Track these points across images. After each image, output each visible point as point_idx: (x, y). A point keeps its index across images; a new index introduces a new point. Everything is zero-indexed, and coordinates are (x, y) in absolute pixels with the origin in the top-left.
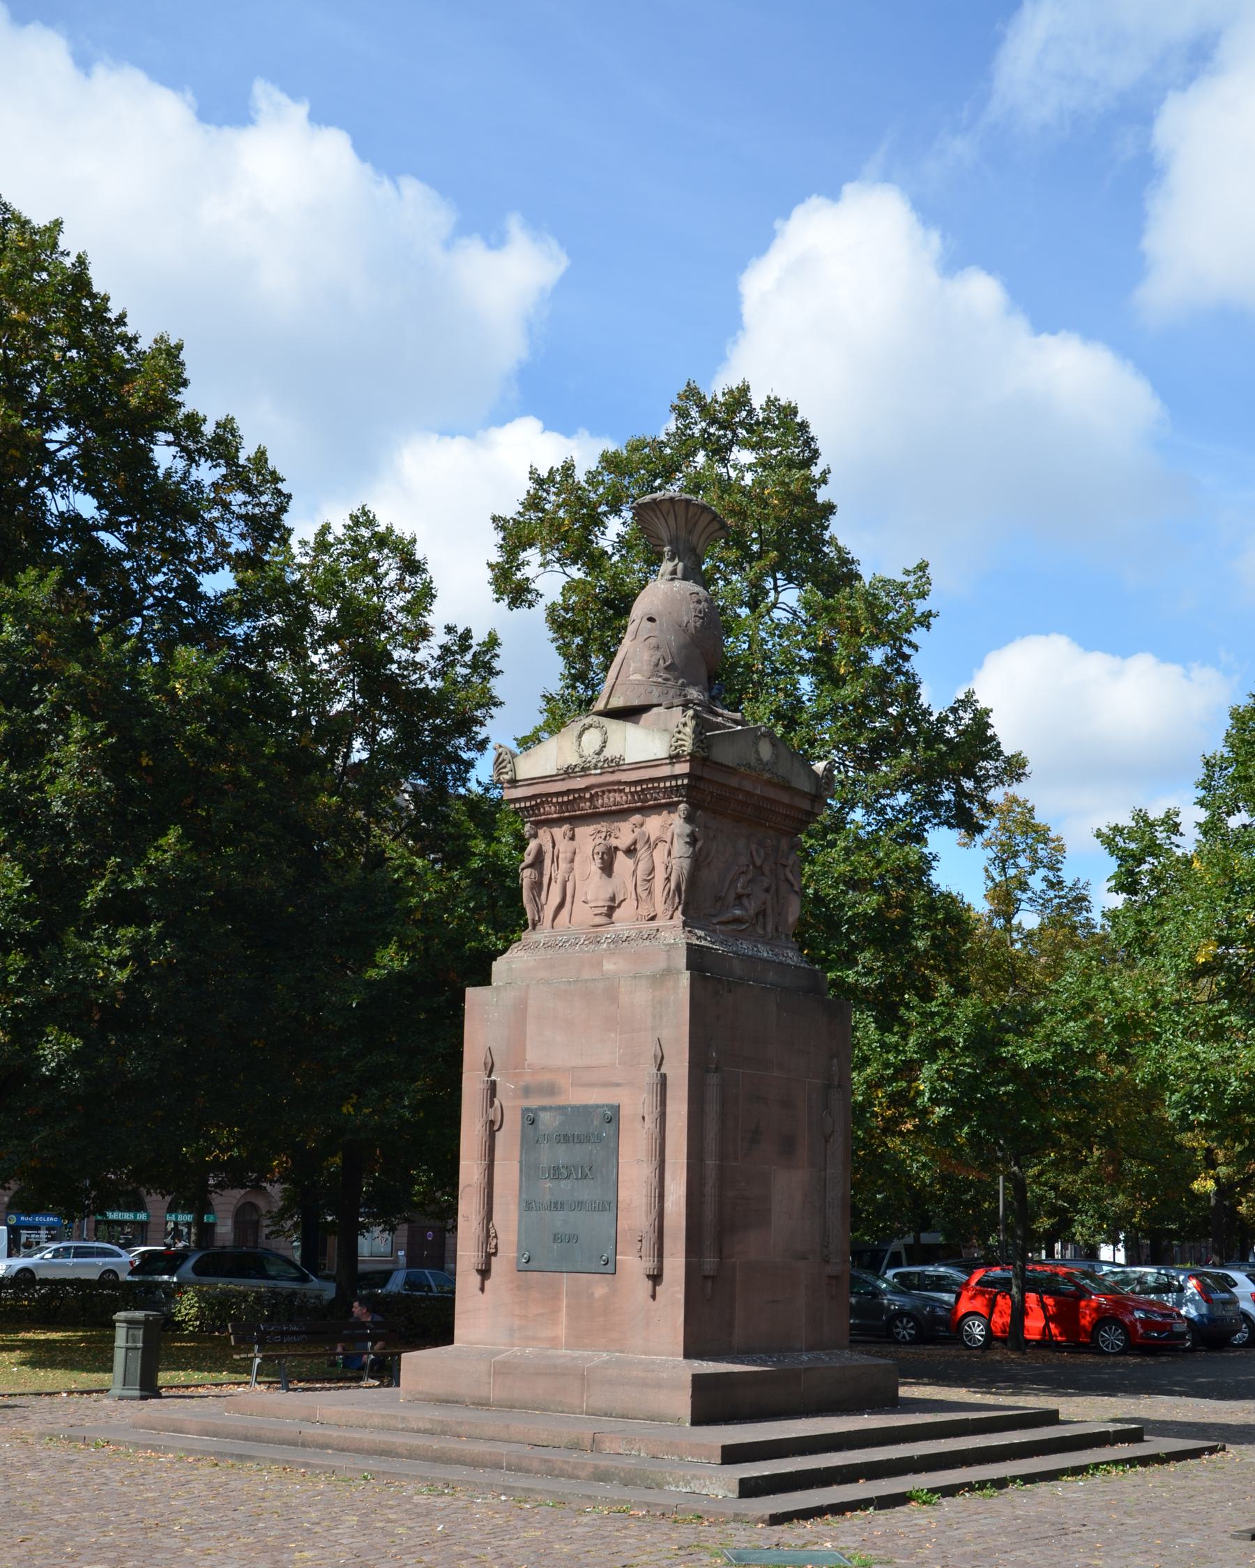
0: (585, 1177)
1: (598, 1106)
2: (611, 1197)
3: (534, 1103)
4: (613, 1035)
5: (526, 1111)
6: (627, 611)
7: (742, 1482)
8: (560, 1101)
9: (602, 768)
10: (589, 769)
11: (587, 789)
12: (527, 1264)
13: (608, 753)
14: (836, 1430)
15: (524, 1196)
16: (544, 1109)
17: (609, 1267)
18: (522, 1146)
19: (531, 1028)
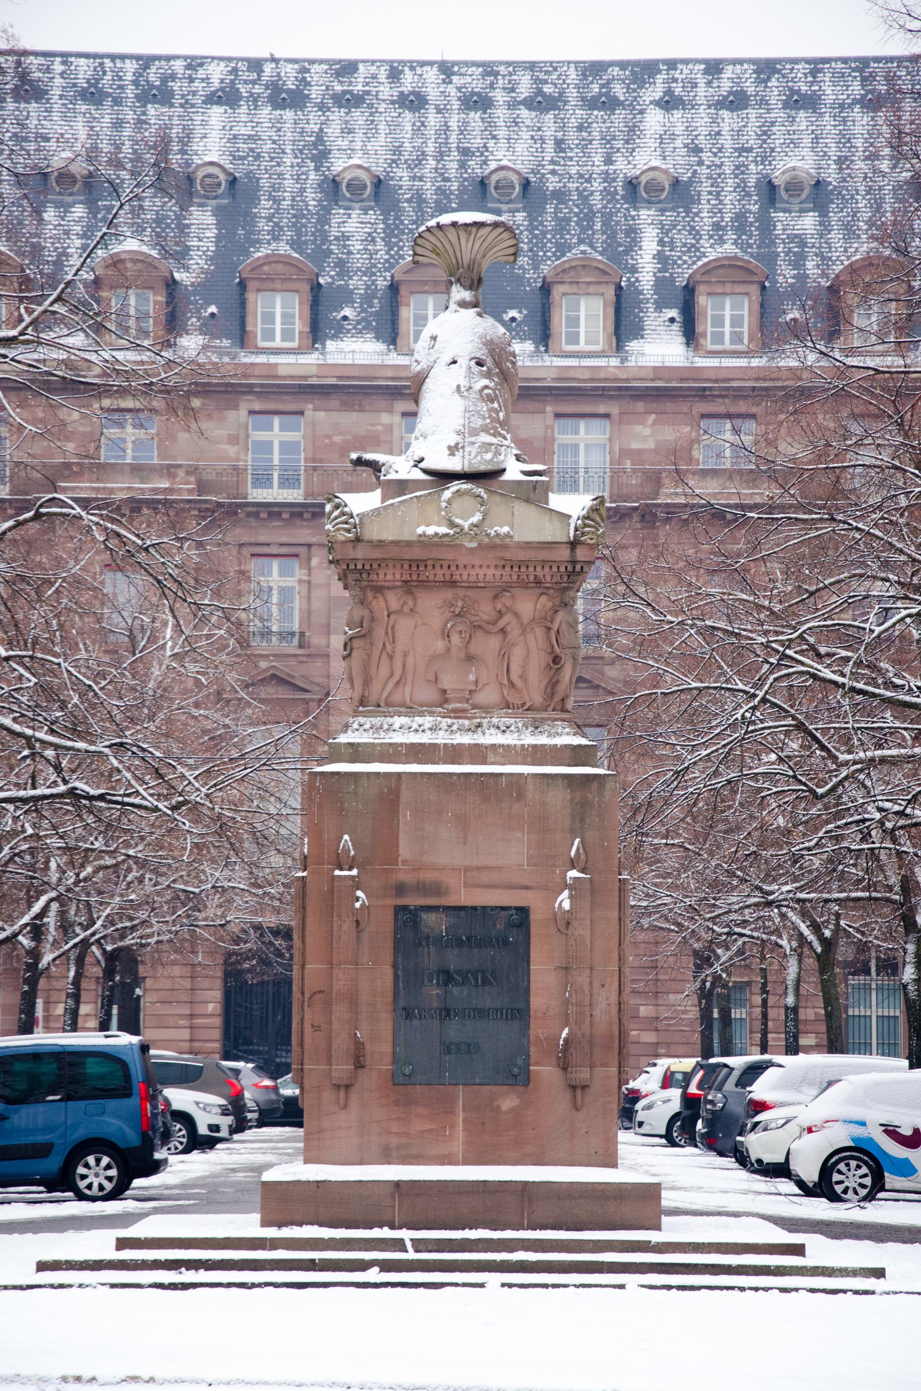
0: (486, 982)
2: (521, 1005)
3: (413, 901)
4: (519, 834)
5: (401, 910)
6: (508, 746)
7: (118, 1239)
8: (452, 901)
12: (402, 1079)
14: (685, 1276)
15: (402, 1003)
19: (406, 817)
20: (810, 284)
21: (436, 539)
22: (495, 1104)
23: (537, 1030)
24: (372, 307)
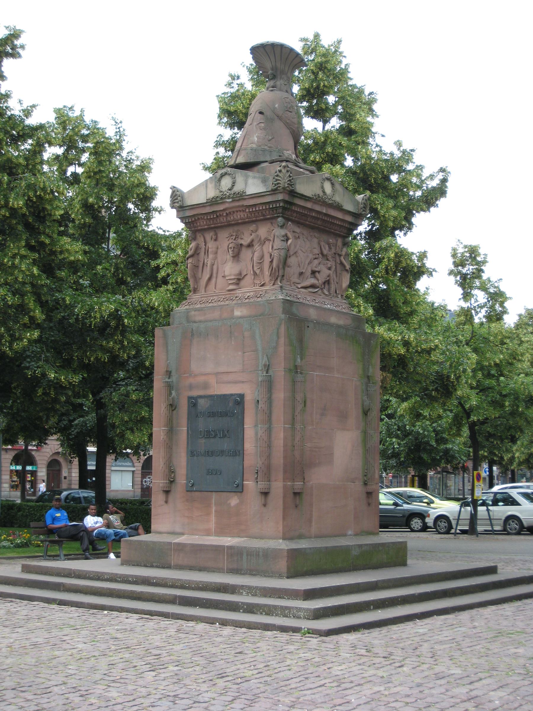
0: (224, 436)
1: (232, 395)
5: (190, 398)
9: (232, 198)
10: (225, 198)
11: (224, 210)
12: (191, 488)
13: (236, 189)
16: (201, 397)
17: (239, 489)
18: (188, 419)
20: (34, 144)
21: (214, 200)
22: (228, 502)
23: (247, 463)
24: (15, 199)
